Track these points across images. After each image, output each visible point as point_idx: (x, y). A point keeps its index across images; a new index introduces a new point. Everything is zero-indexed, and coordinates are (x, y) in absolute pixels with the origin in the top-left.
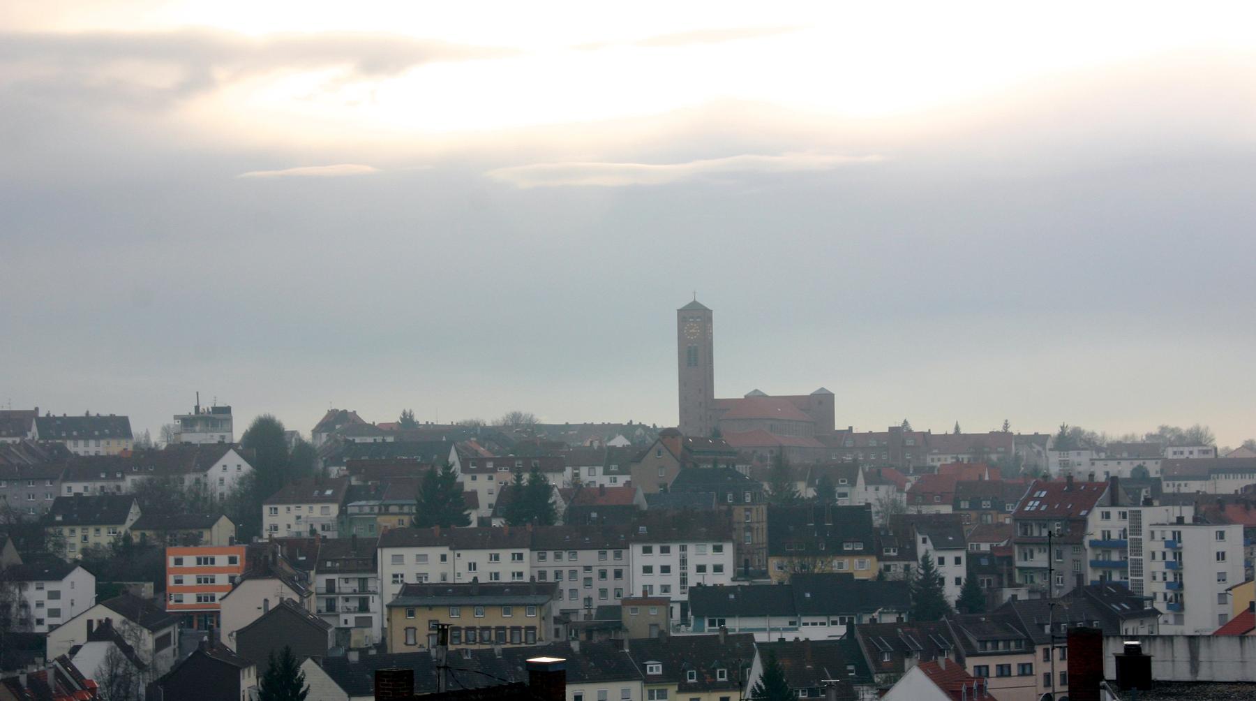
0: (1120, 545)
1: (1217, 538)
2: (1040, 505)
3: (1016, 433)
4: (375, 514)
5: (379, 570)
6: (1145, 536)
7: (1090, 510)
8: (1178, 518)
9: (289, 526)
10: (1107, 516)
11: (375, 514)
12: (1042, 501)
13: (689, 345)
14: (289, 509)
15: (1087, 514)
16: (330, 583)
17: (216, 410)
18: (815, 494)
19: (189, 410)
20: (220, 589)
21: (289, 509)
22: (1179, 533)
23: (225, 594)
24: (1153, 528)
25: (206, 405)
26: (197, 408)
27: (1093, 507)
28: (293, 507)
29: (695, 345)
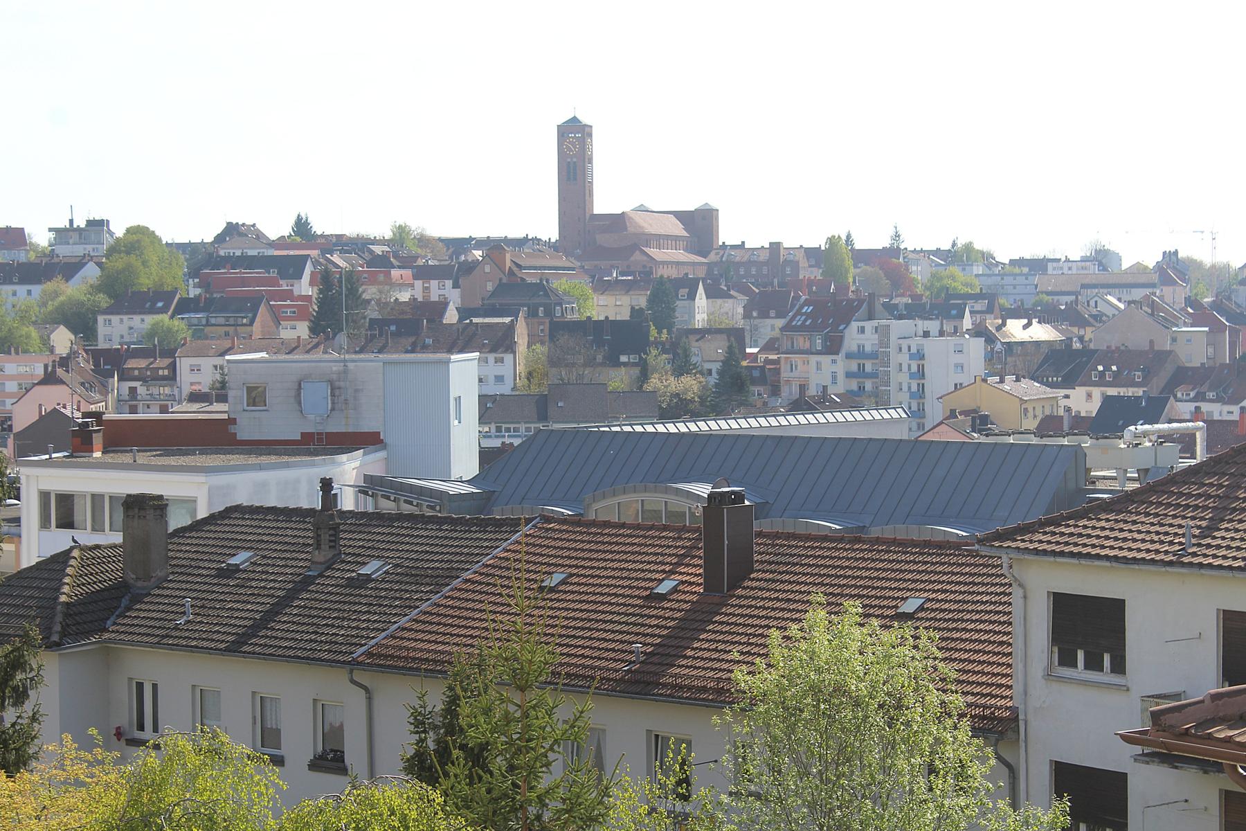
0: (873, 356)
1: (155, 687)
2: (805, 320)
3: (319, 233)
4: (202, 325)
5: (178, 379)
6: (892, 350)
7: (848, 324)
8: (924, 332)
9: (122, 337)
10: (862, 330)
11: (202, 325)
12: (808, 315)
13: (569, 160)
14: (122, 320)
15: (845, 328)
16: (133, 390)
17: (91, 223)
18: (1125, 266)
19: (63, 223)
20: (11, 395)
21: (122, 320)
22: (864, 365)
23: (15, 400)
24: (901, 341)
25: (80, 222)
26: (71, 221)
27: (850, 321)
28: (125, 318)
29: (575, 160)
